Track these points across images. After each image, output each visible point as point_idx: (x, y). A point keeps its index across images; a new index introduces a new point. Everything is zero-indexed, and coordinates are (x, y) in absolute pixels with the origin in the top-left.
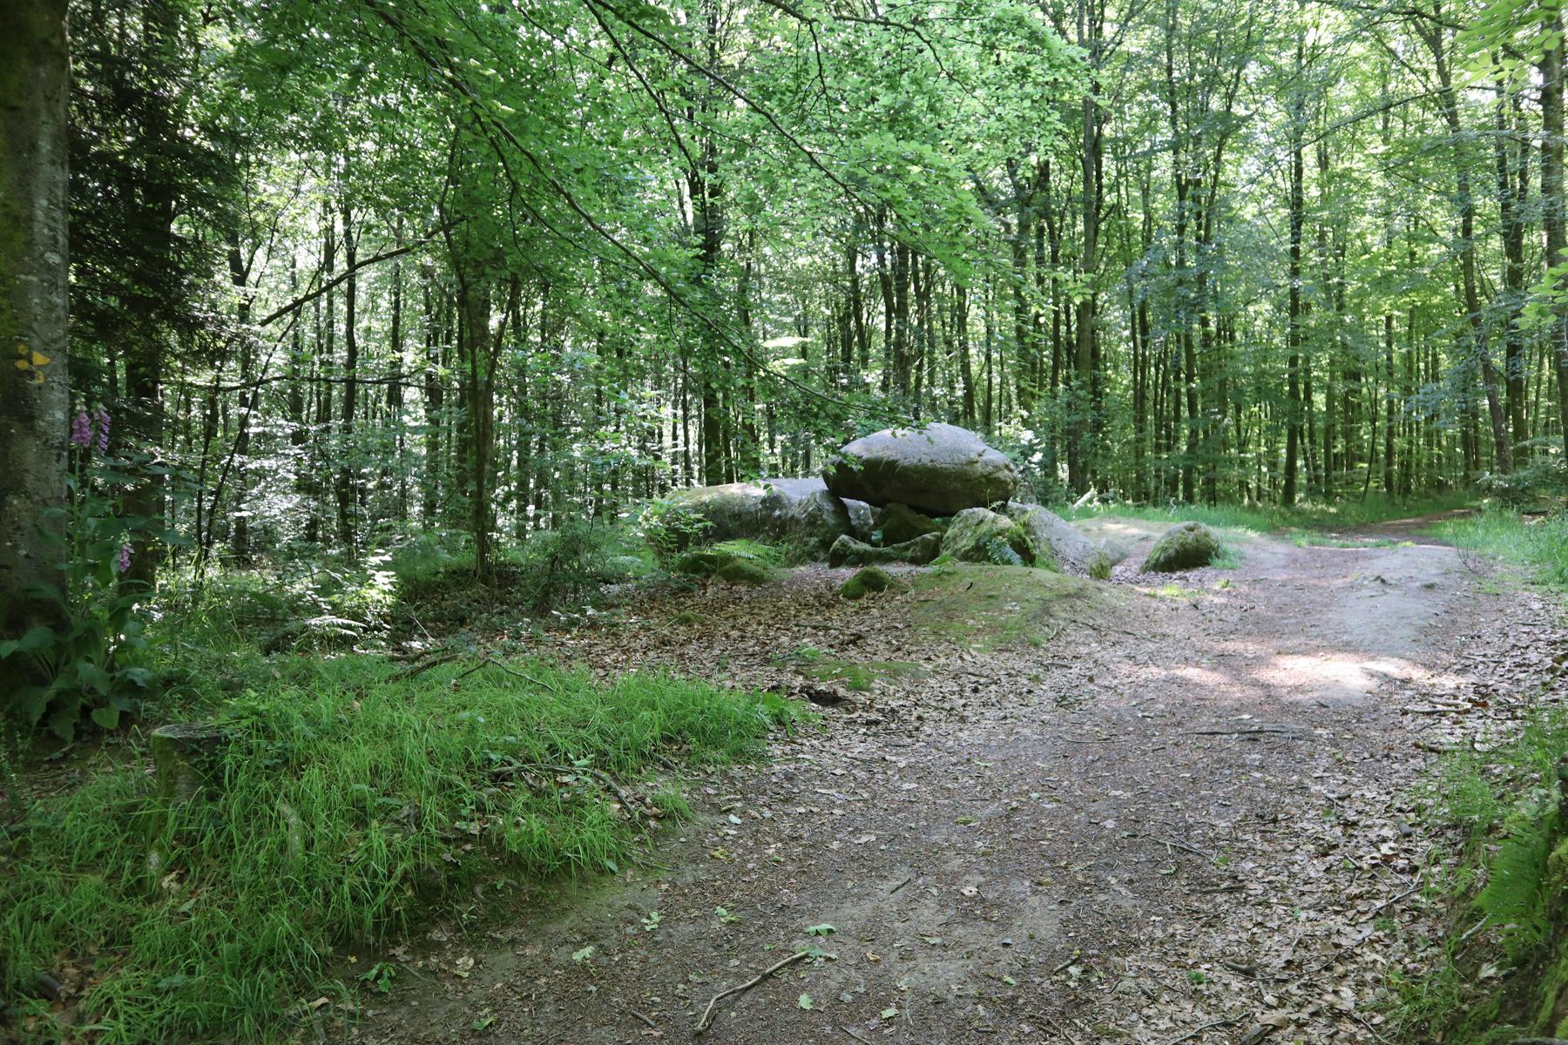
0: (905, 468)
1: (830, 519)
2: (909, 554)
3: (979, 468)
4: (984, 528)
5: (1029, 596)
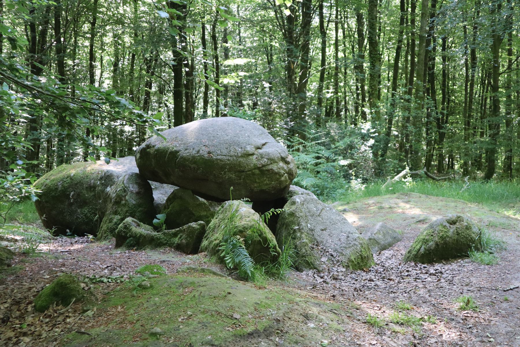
0: (184, 159)
1: (131, 200)
2: (176, 240)
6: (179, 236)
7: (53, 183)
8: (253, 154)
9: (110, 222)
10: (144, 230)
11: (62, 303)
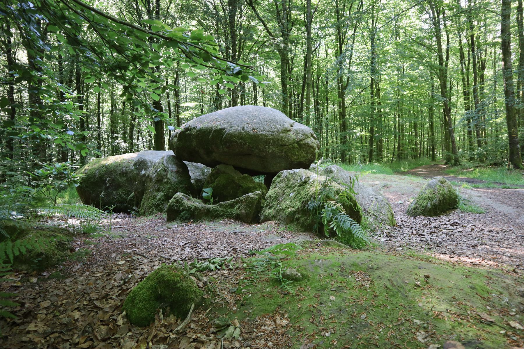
0: (231, 135)
1: (172, 177)
2: (234, 211)
3: (292, 135)
6: (237, 207)
7: (91, 171)
8: (290, 131)
9: (154, 199)
10: (196, 203)
11: (172, 311)
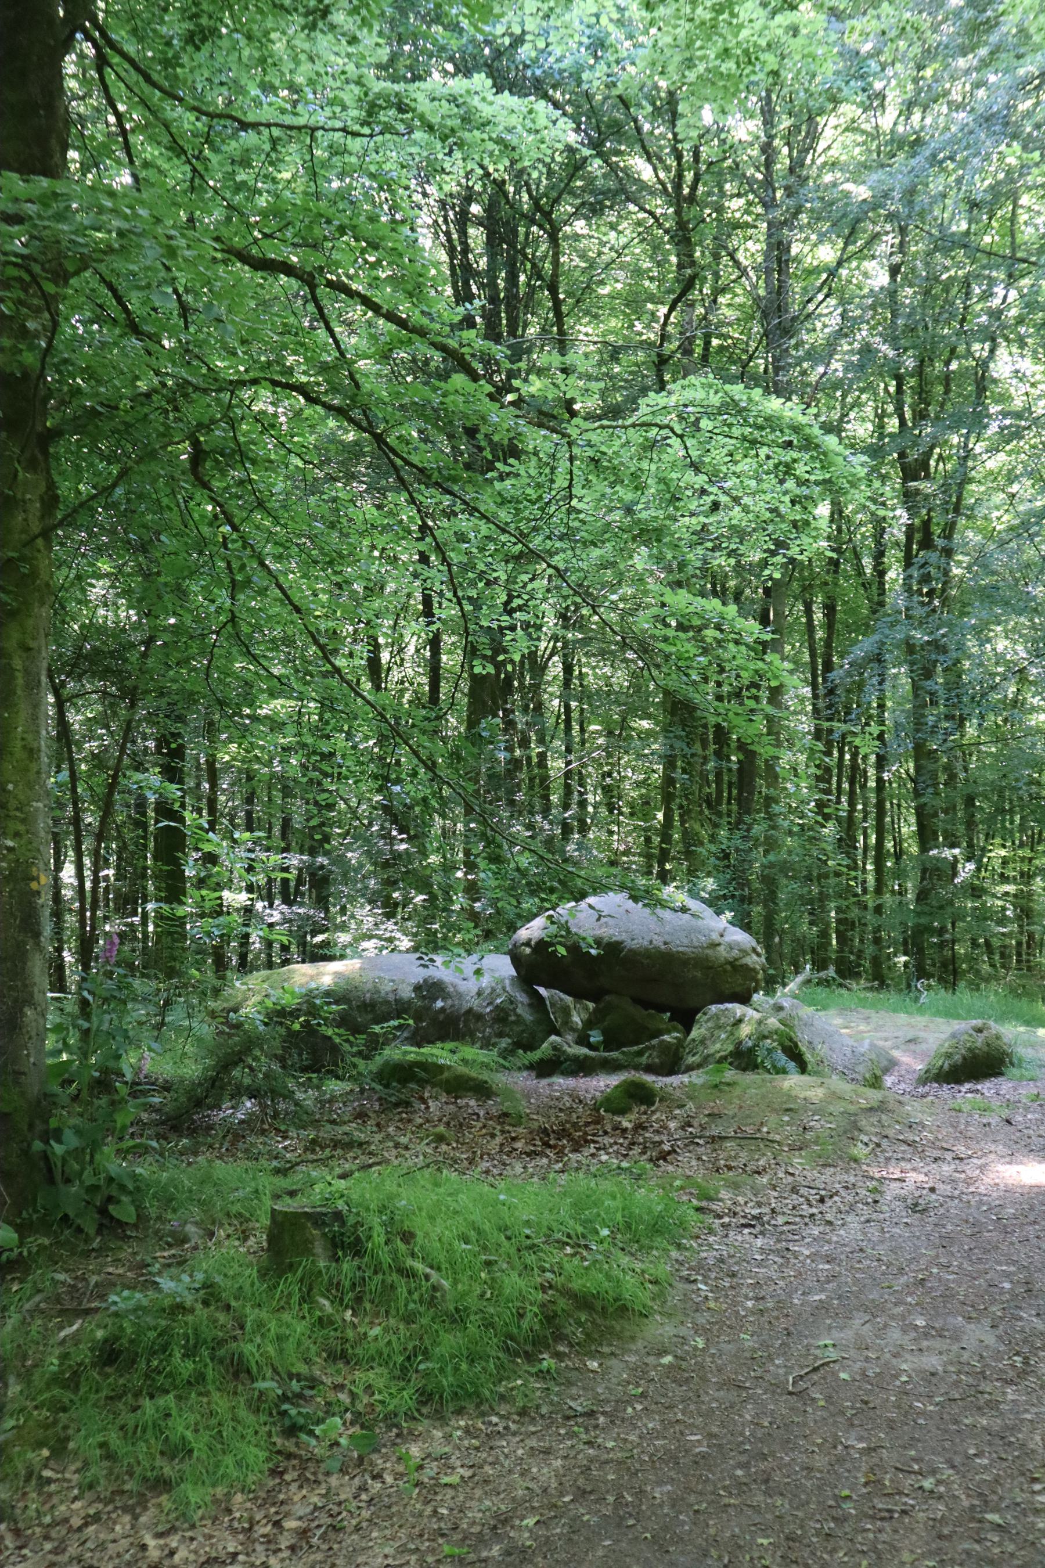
2: (644, 1060)
3: (722, 952)
4: (745, 1030)
5: (831, 1109)
